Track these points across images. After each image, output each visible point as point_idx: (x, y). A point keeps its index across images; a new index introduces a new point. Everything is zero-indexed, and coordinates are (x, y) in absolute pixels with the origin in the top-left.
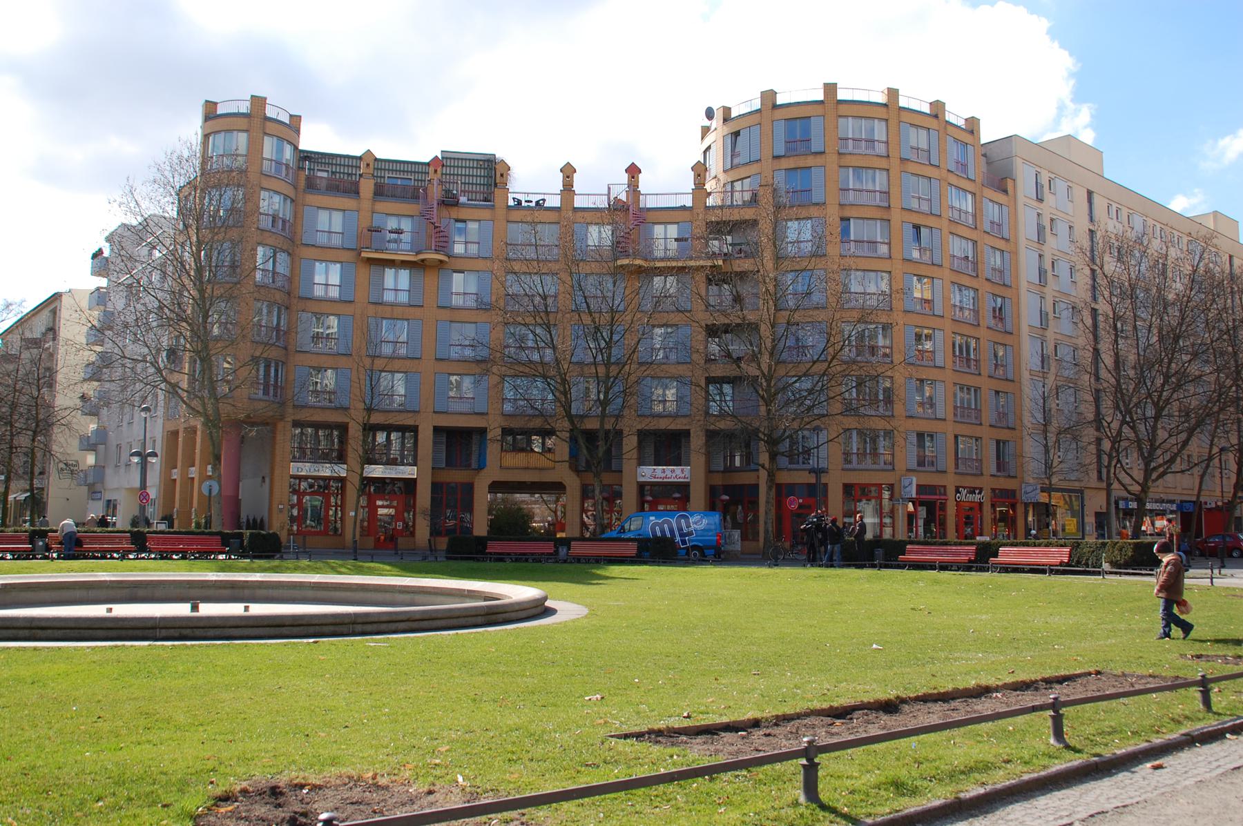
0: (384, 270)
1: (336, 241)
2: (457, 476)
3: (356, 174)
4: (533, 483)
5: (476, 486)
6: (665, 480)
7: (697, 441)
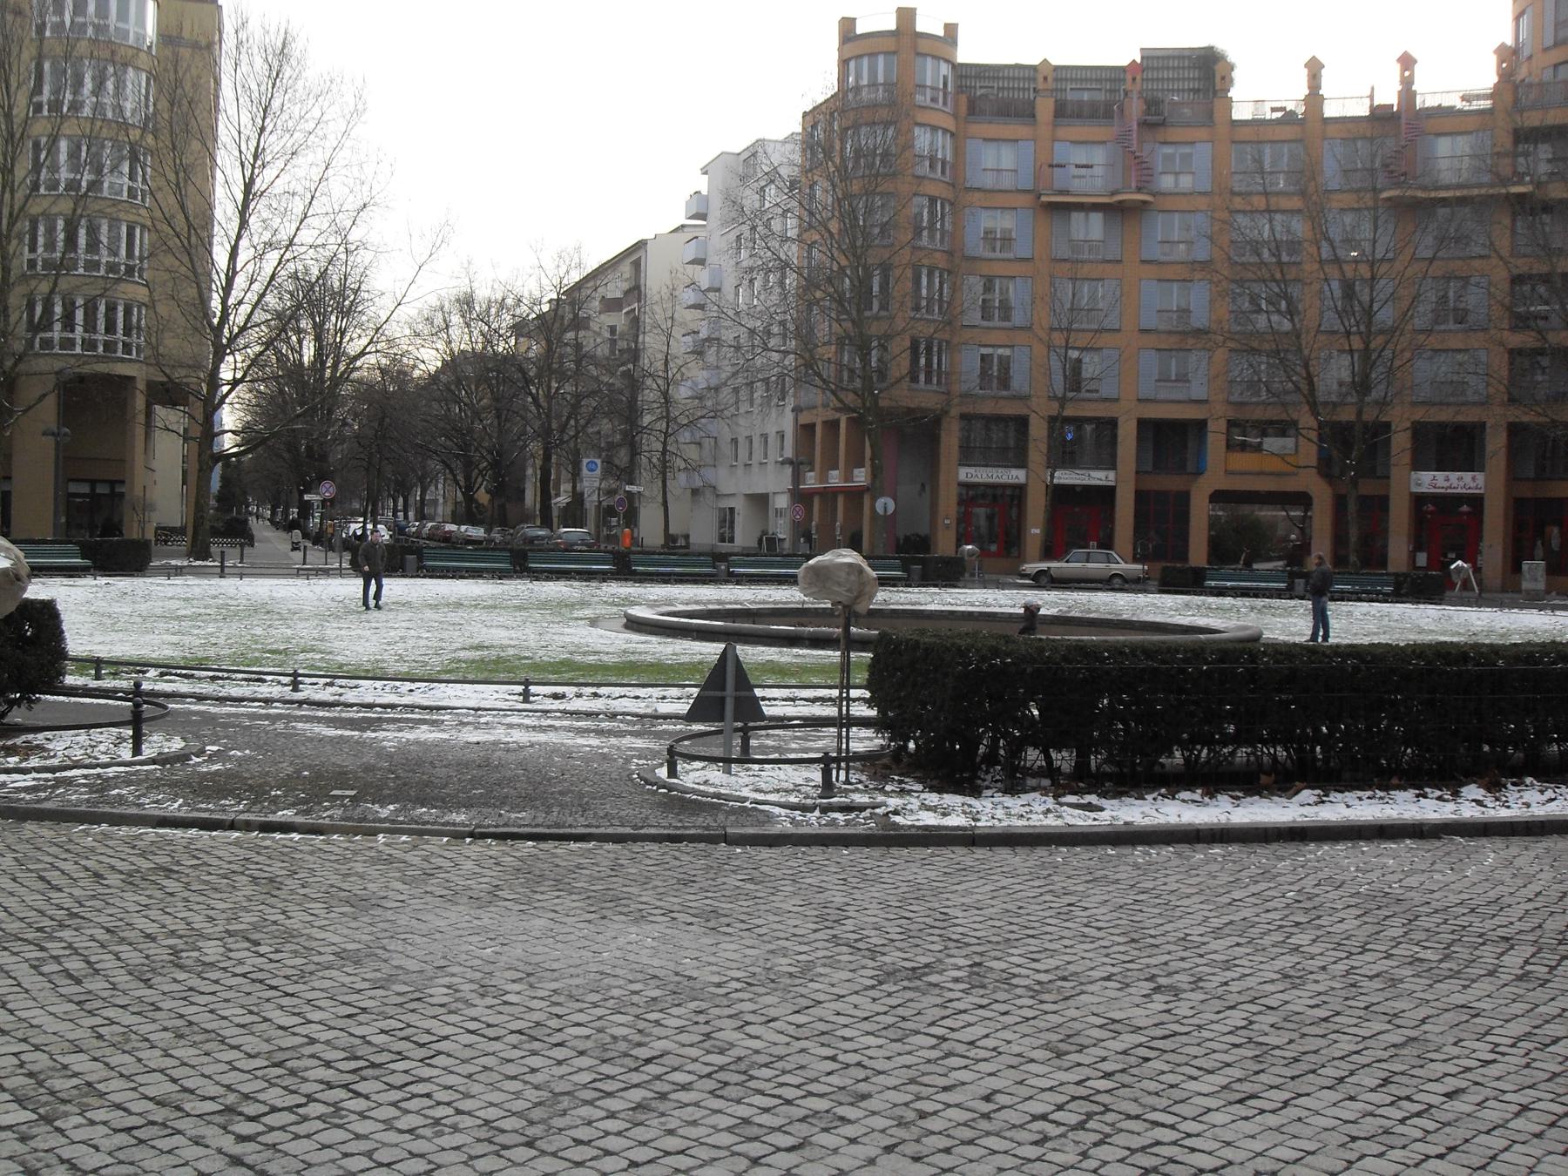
1: (1007, 182)
2: (1168, 482)
4: (1269, 493)
5: (1192, 497)
7: (1496, 443)
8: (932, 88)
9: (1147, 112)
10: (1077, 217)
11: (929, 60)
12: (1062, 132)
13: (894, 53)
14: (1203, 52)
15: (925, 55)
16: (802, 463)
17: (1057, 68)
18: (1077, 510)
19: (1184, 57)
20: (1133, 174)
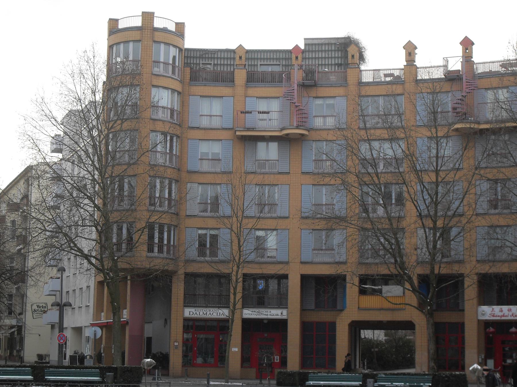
0: (256, 143)
1: (216, 123)
2: (324, 316)
4: (389, 322)
5: (337, 325)
6: (503, 318)
8: (164, 63)
9: (306, 78)
10: (261, 146)
11: (162, 46)
13: (139, 41)
14: (343, 41)
15: (159, 42)
17: (248, 52)
18: (266, 335)
19: (332, 44)
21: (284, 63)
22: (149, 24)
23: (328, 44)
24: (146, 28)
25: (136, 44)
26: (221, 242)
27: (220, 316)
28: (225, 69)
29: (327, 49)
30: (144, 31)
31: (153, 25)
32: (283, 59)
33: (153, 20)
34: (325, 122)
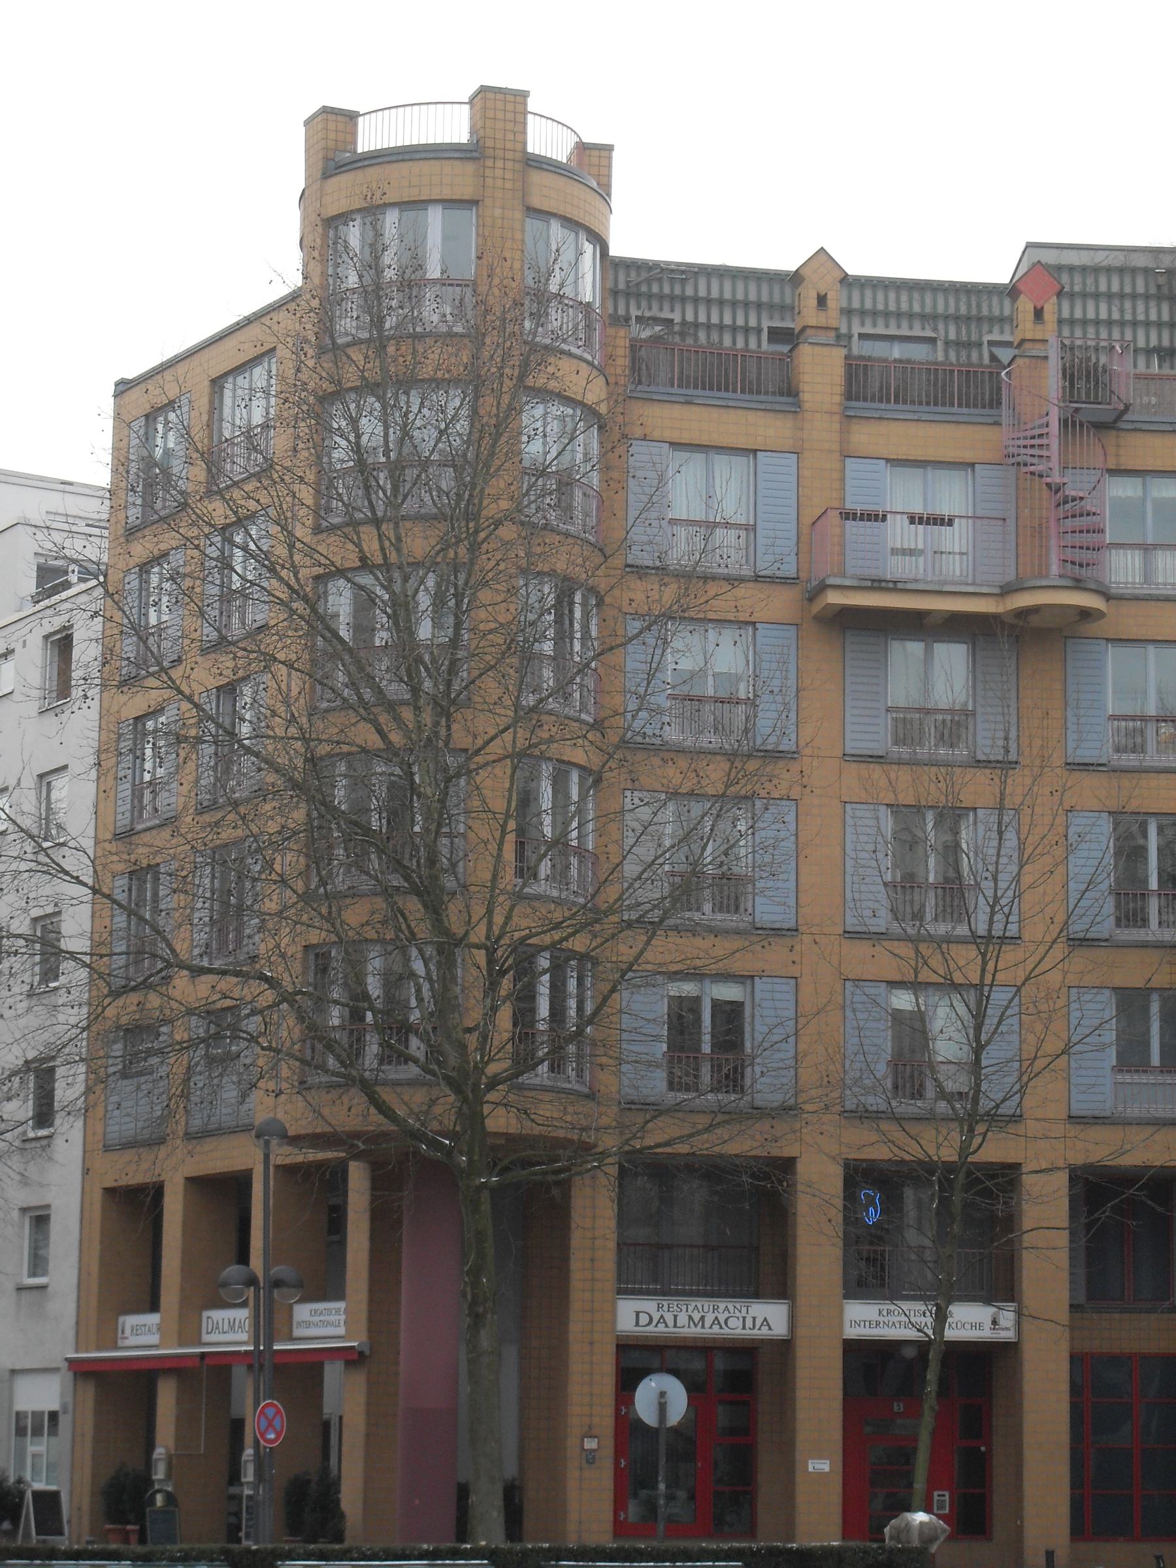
3: (759, 331)
12: (864, 436)
13: (473, 203)
16: (277, 1283)
19: (1134, 271)
20: (1053, 542)
21: (952, 336)
22: (510, 136)
23: (1121, 270)
24: (499, 153)
25: (460, 215)
26: (756, 1030)
27: (756, 1331)
28: (740, 344)
29: (1115, 288)
30: (489, 163)
31: (525, 143)
32: (946, 317)
33: (525, 124)
34: (1148, 573)
